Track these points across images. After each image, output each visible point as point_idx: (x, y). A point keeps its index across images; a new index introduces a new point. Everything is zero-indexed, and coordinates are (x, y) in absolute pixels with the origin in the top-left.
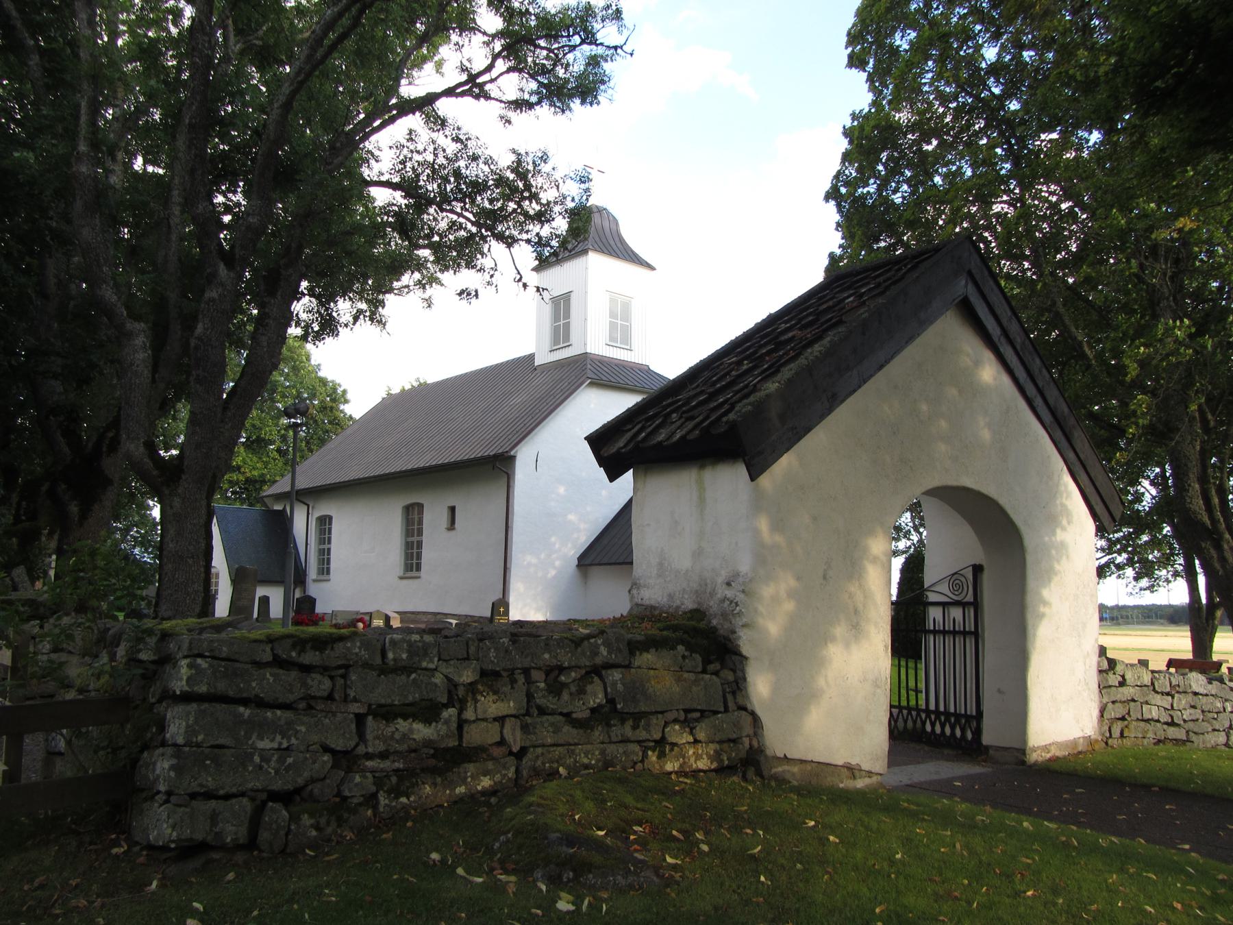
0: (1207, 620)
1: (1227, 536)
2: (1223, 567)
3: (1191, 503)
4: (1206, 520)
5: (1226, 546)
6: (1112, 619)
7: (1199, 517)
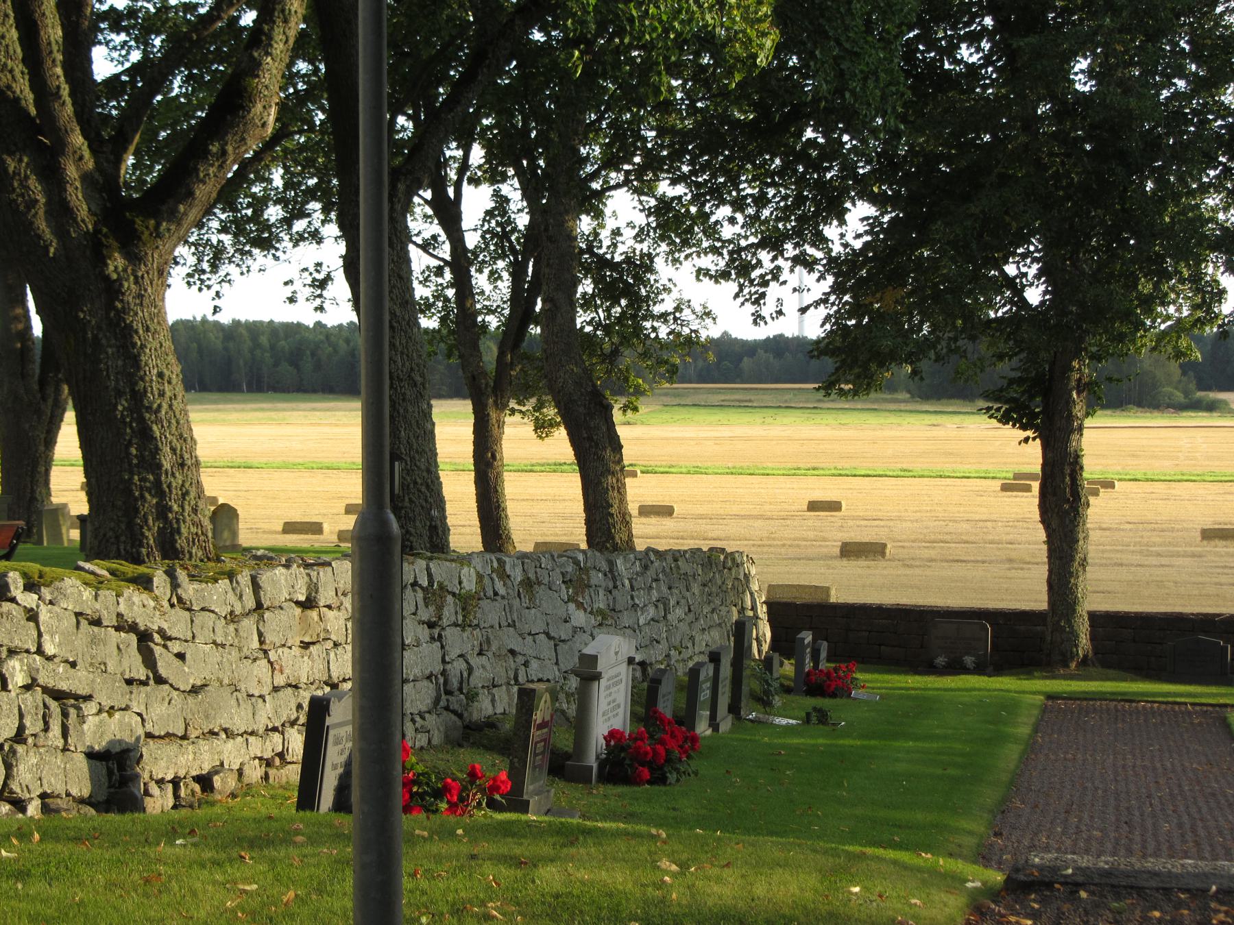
0: (42, 383)
1: (78, 139)
2: (61, 233)
4: (23, 89)
5: (72, 172)
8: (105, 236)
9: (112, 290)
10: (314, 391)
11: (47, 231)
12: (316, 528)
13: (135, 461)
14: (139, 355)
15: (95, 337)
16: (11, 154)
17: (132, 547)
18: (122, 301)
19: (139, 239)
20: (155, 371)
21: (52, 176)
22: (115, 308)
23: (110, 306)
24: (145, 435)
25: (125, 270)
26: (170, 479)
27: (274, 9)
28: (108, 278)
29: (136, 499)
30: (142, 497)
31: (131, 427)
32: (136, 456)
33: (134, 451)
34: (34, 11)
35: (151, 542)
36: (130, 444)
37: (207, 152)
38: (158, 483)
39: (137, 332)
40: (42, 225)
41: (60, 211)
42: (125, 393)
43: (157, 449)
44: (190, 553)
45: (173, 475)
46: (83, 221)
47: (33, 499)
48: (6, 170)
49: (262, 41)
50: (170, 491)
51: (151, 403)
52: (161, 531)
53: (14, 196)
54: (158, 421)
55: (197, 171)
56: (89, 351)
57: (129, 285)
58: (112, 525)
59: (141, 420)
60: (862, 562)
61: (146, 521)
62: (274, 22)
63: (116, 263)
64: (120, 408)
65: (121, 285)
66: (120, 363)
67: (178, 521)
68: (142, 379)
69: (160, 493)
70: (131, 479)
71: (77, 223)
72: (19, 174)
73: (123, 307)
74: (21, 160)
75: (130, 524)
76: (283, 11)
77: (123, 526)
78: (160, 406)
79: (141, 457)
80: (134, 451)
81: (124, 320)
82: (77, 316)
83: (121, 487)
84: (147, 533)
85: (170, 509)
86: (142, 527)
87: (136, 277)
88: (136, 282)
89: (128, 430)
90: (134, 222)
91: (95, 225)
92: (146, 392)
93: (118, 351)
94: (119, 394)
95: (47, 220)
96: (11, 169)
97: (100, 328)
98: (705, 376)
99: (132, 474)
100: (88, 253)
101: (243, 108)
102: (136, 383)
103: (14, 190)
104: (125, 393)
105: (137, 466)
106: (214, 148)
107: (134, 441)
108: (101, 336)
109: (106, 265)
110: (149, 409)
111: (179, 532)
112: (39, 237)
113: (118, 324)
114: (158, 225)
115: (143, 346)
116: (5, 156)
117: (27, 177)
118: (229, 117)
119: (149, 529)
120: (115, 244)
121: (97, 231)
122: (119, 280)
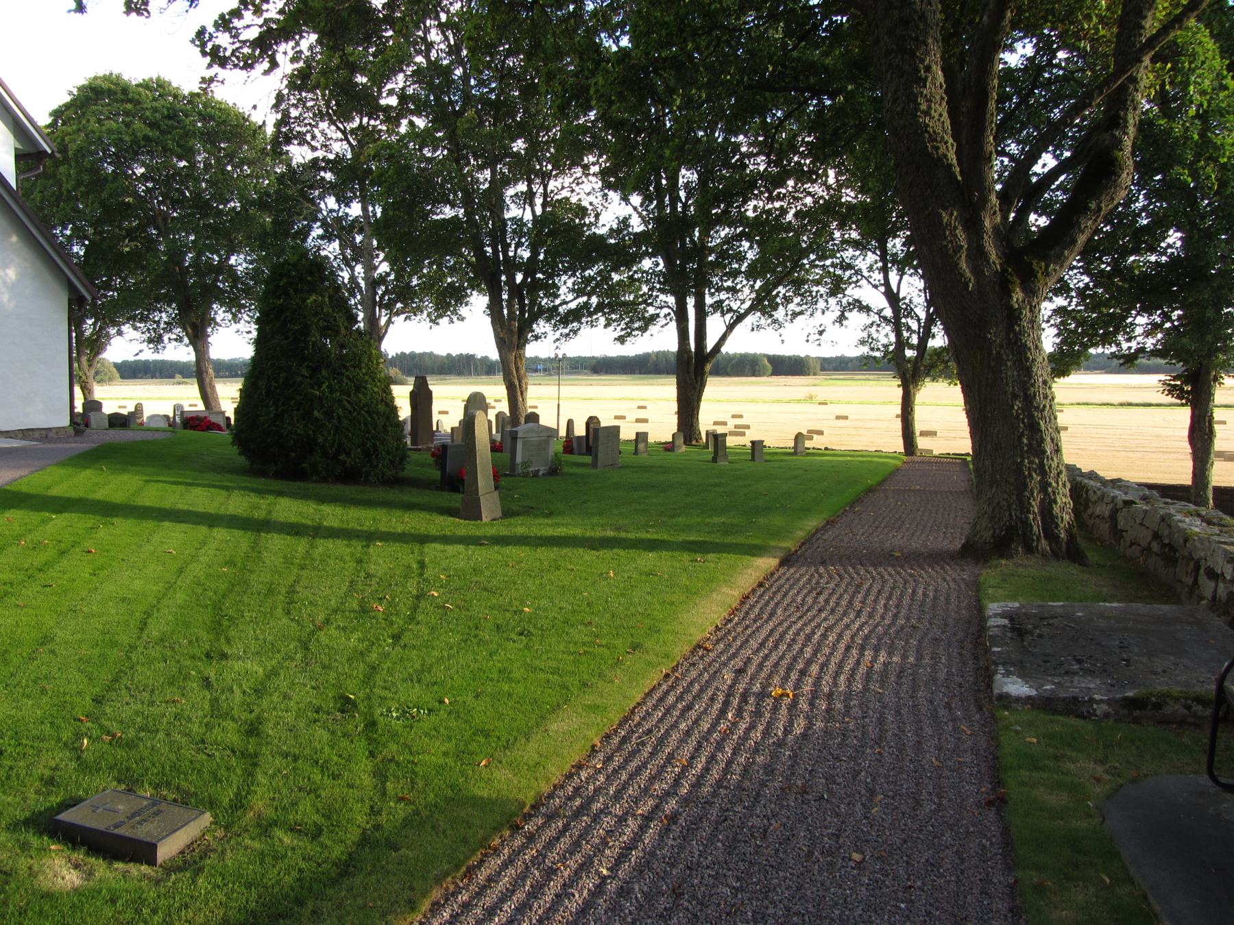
2: (977, 272)
3: (927, 113)
6: (545, 370)
7: (942, 149)
8: (1012, 275)
9: (1013, 316)
10: (663, 373)
11: (967, 270)
12: (725, 424)
13: (1026, 448)
14: (1031, 367)
15: (998, 353)
16: (945, 209)
17: (1022, 513)
18: (1019, 325)
19: (1036, 277)
20: (1040, 380)
21: (973, 226)
22: (1014, 331)
23: (1010, 329)
24: (1034, 428)
25: (1023, 301)
26: (1050, 461)
27: (1127, 100)
28: (1011, 307)
29: (1025, 477)
30: (1030, 475)
31: (1023, 422)
32: (1026, 445)
33: (1025, 441)
34: (988, 84)
35: (1036, 510)
36: (1022, 435)
37: (1087, 208)
38: (1042, 465)
39: (1030, 349)
40: (963, 265)
41: (978, 254)
42: (1019, 396)
43: (1042, 440)
44: (1062, 518)
45: (1052, 459)
46: (994, 263)
47: (692, 425)
48: (247, 395)
49: (1119, 124)
50: (1051, 472)
51: (1039, 405)
52: (1042, 501)
53: (945, 243)
54: (1043, 418)
55: (1079, 224)
56: (993, 364)
57: (1026, 312)
58: (1005, 496)
59: (1031, 416)
60: (928, 438)
61: (1032, 494)
62: (1127, 110)
63: (1018, 295)
64: (1016, 408)
65: (1021, 313)
66: (1015, 373)
67: (1054, 493)
68: (1033, 385)
69: (1043, 471)
70: (1022, 461)
71: (990, 265)
72: (950, 225)
73: (1020, 330)
74: (952, 214)
75: (1020, 497)
76: (1133, 101)
77: (1014, 497)
78: (1044, 406)
79: (1029, 446)
80: (1025, 441)
81: (1021, 340)
82: (985, 337)
83: (1014, 467)
84: (1033, 503)
85: (1050, 485)
86: (1029, 499)
87: (1031, 306)
88: (1031, 311)
89: (1021, 425)
90: (1032, 264)
91: (1001, 265)
92: (1035, 395)
93: (1014, 364)
94: (1015, 397)
95: (967, 263)
96: (945, 220)
97: (1001, 346)
98: (836, 369)
99: (1023, 458)
100: (997, 288)
101: (1115, 173)
102: (1029, 389)
103: (946, 238)
104: (1019, 396)
105: (1027, 452)
106: (1093, 205)
107: (1026, 433)
108: (1002, 352)
109: (1011, 297)
110: (1037, 408)
111: (1055, 501)
112: (962, 275)
113: (1016, 343)
114: (1047, 266)
115: (1034, 360)
116: (940, 211)
117: (956, 228)
118: (1104, 181)
119: (1034, 500)
120: (1018, 281)
121: (1004, 271)
122: (1020, 309)
